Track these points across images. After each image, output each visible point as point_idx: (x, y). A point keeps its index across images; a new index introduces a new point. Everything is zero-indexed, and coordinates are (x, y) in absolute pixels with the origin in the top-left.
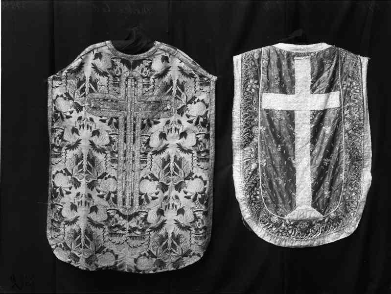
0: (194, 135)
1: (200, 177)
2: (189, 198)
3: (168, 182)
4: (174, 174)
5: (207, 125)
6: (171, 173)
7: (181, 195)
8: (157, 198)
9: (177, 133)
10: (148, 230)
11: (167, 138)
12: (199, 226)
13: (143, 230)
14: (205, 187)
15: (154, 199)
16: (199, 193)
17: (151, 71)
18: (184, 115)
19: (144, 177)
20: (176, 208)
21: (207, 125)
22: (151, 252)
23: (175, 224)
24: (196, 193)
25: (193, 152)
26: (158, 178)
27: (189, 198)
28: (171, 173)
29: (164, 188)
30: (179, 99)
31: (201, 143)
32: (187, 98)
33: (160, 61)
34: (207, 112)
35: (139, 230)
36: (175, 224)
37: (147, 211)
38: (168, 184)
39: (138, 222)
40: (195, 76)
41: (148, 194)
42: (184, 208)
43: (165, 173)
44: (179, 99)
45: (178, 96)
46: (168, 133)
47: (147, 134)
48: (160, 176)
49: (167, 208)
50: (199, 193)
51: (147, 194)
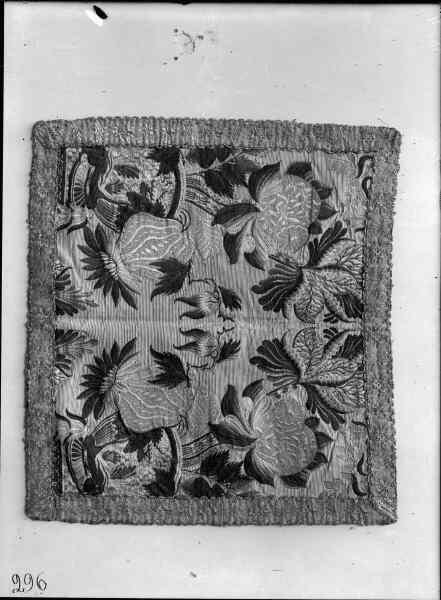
0: (168, 419)
1: (319, 459)
2: (229, 406)
3: (302, 316)
4: (333, 335)
5: (211, 482)
6: (341, 326)
7: (239, 371)
8: (233, 259)
9: (183, 340)
10: (95, 222)
11: (159, 298)
12: (105, 457)
13: (91, 200)
14: (277, 480)
15: (231, 243)
16: (249, 455)
17: (125, 213)
18: (258, 373)
19: (332, 201)
20: (187, 346)
21: (211, 482)
22: (337, 241)
23: (115, 346)
24: (250, 441)
25: (91, 417)
26: (321, 264)
27: (229, 406)
28: (341, 326)
29: (276, 295)
30: (327, 347)
31: (135, 455)
32: (330, 385)
33: (167, 254)
34: (265, 479)
35: (93, 180)
36: (115, 346)
37: (177, 215)
38: (291, 314)
39: (132, 172)
40: (91, 417)
41: (254, 214)
42: (184, 384)
43: (345, 298)
44: (327, 347)
45: (342, 341)
46: (182, 300)
47: (181, 204)
48: (330, 275)
49: (186, 308)
50: (249, 455)
51: (257, 210)
